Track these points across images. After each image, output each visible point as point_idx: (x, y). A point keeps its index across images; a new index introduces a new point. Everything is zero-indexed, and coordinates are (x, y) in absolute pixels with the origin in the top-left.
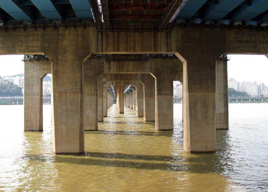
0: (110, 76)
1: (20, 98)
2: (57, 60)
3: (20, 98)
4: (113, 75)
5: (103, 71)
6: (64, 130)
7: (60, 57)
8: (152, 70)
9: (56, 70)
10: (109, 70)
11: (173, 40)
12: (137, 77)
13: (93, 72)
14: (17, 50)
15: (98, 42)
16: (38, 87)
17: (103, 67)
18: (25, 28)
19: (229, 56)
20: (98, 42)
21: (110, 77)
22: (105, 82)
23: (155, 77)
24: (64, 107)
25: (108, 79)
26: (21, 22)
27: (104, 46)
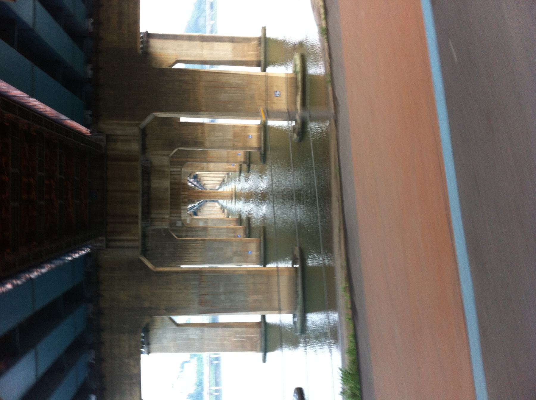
0: (173, 215)
1: (101, 137)
2: (150, 308)
3: (101, 137)
4: (172, 210)
5: (166, 230)
6: (255, 297)
7: (146, 305)
8: (165, 154)
9: (166, 309)
10: (163, 221)
11: (119, 132)
12: (175, 173)
13: (167, 246)
14: (135, 371)
15: (123, 247)
16: (331, 88)
17: (159, 231)
18: (100, 360)
19: (140, 32)
20: (123, 247)
21: (176, 215)
22: (183, 224)
23: (176, 150)
24: (222, 297)
25: (177, 218)
26: (91, 366)
27: (129, 238)
